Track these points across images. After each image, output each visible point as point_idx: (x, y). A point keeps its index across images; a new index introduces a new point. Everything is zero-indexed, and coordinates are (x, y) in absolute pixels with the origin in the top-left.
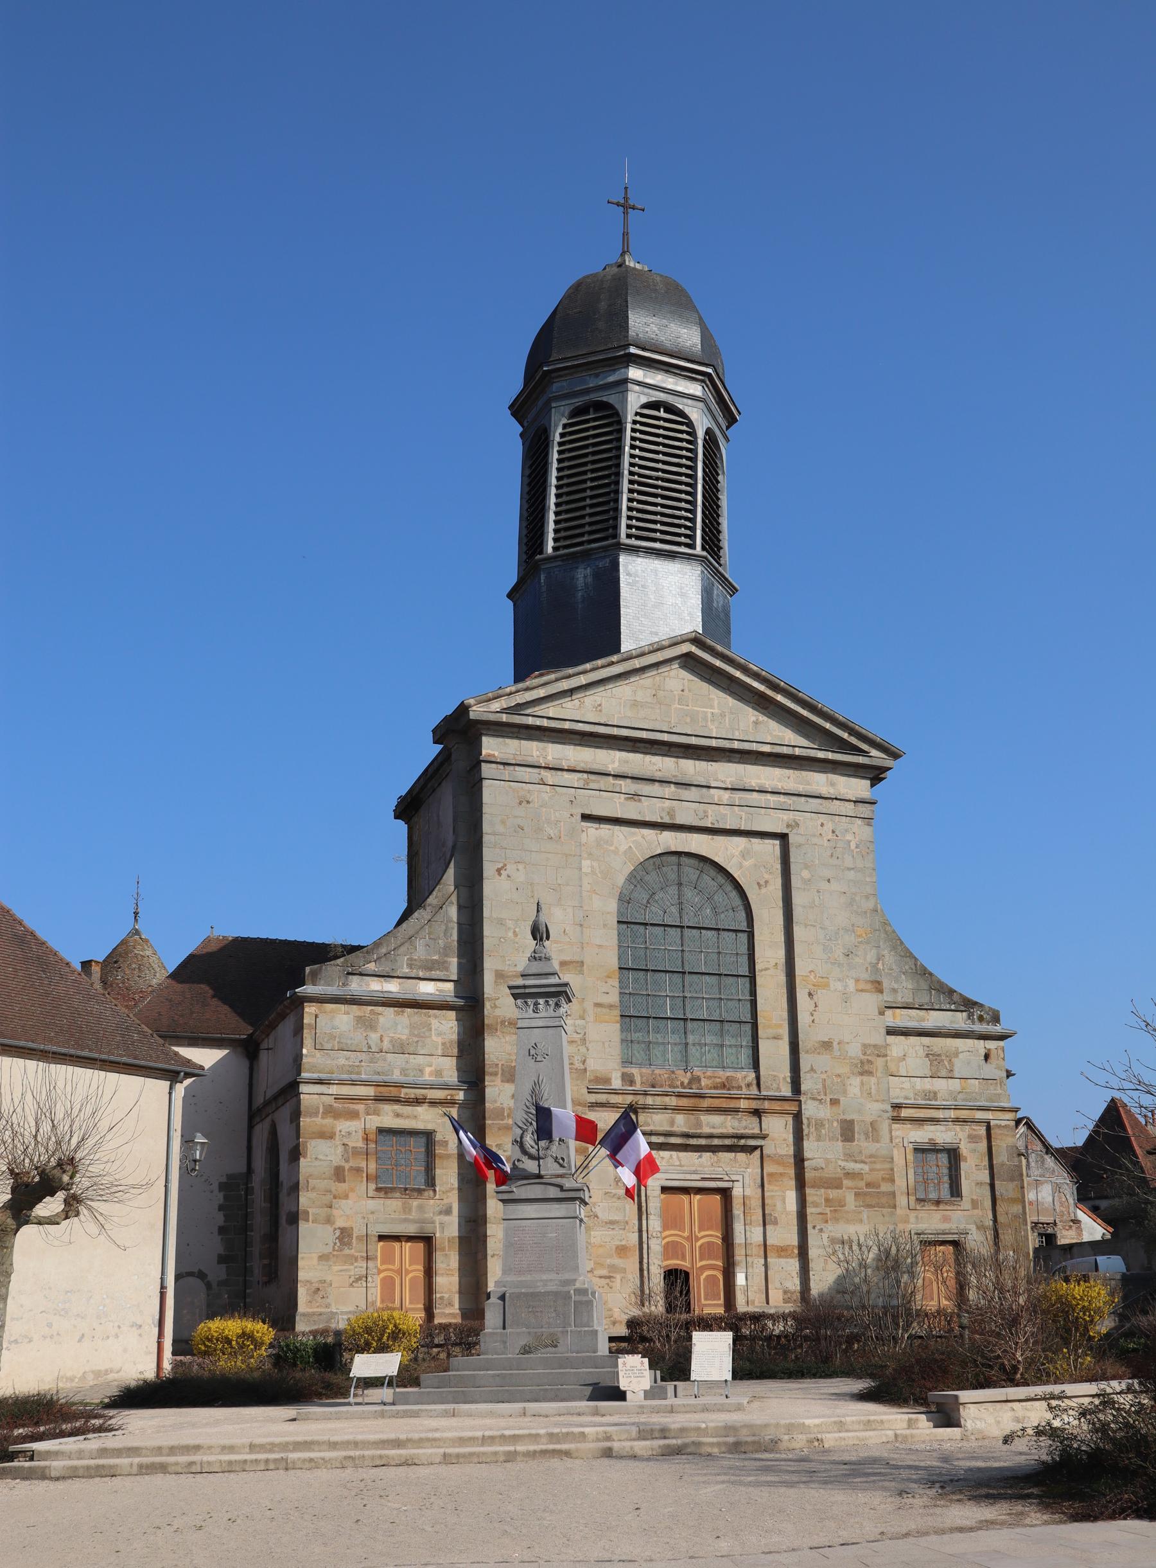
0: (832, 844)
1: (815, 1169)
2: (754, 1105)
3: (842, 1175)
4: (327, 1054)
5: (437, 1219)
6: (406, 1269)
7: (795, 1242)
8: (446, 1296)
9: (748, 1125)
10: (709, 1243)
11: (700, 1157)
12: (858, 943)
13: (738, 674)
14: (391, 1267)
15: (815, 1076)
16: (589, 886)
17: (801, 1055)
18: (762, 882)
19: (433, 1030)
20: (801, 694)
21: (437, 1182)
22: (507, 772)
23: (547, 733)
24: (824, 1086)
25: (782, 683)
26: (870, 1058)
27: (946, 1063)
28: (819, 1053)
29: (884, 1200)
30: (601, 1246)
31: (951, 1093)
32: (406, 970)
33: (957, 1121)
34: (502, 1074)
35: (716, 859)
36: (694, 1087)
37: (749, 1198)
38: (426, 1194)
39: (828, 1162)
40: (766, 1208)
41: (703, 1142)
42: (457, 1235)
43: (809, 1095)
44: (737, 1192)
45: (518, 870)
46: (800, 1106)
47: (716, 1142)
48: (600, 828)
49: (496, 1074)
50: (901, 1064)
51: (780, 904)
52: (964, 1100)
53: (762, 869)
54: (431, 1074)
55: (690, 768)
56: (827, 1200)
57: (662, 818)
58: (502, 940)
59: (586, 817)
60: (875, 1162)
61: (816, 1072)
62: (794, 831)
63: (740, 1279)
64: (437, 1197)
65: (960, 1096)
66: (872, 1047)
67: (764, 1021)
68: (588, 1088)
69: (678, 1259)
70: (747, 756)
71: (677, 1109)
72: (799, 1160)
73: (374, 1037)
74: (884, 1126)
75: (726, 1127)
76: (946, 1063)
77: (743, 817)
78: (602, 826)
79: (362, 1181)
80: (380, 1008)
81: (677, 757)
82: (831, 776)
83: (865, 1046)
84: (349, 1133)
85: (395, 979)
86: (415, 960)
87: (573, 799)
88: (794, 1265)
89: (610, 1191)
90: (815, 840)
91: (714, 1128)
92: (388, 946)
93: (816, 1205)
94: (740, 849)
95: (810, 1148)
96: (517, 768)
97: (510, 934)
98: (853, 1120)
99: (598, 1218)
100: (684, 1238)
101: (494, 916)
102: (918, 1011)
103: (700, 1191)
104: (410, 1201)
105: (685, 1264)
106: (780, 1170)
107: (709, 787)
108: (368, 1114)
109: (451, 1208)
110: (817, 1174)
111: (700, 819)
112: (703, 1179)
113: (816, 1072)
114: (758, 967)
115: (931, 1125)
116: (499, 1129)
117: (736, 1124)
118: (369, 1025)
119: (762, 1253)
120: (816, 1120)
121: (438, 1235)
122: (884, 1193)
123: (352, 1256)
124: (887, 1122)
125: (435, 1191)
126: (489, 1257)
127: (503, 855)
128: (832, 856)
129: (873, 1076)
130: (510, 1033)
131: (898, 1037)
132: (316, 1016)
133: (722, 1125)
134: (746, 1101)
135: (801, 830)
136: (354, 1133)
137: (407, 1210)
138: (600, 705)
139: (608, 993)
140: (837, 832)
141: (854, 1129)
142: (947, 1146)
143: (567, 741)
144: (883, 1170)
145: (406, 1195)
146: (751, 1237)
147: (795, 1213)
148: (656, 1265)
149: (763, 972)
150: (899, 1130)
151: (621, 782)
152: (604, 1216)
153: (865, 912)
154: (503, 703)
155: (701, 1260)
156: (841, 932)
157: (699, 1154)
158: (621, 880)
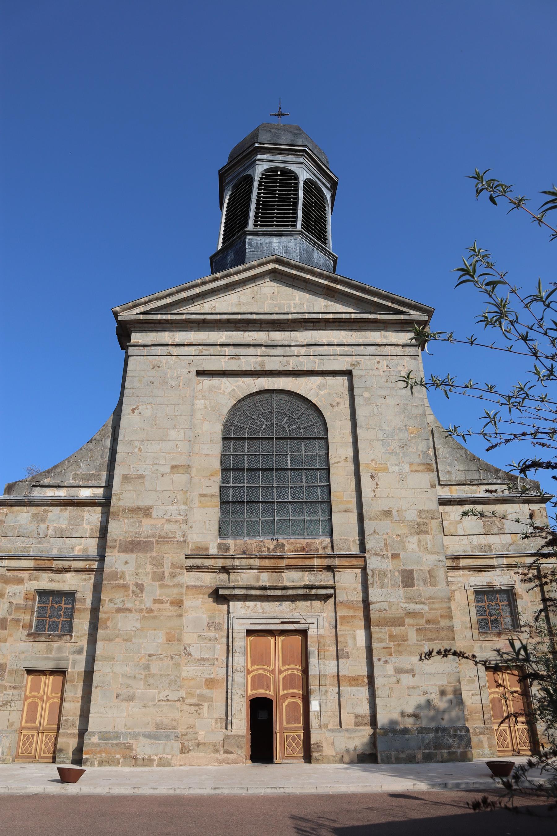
0: (386, 374)
1: (380, 611)
2: (326, 562)
3: (404, 615)
4: (9, 540)
5: (71, 657)
6: (47, 697)
7: (365, 673)
8: (71, 718)
9: (325, 578)
10: (290, 675)
11: (281, 605)
12: (411, 437)
13: (308, 276)
14: (36, 694)
15: (378, 537)
16: (202, 416)
17: (365, 522)
18: (334, 404)
19: (85, 520)
20: (353, 281)
21: (74, 629)
22: (145, 351)
23: (174, 325)
24: (386, 545)
25: (339, 277)
26: (425, 521)
27: (498, 523)
28: (381, 520)
29: (443, 634)
30: (192, 679)
31: (503, 545)
32: (71, 482)
33: (509, 566)
34: (119, 546)
35: (299, 392)
36: (278, 551)
37: (324, 637)
38: (64, 638)
39: (391, 604)
40: (339, 644)
41: (279, 592)
42: (83, 669)
43: (373, 552)
44: (312, 632)
45: (147, 409)
46: (365, 561)
47: (290, 592)
48: (212, 380)
49: (114, 547)
50: (458, 526)
51: (349, 417)
52: (514, 550)
53: (335, 396)
54: (79, 551)
55: (277, 337)
56: (391, 636)
57: (255, 368)
58: (130, 454)
59: (200, 373)
60: (433, 603)
61: (378, 534)
62: (357, 368)
63: (314, 706)
64: (73, 640)
65: (511, 548)
66: (426, 513)
67: (336, 499)
68: (186, 555)
69: (263, 689)
70: (318, 324)
71: (261, 569)
72: (366, 603)
73: (43, 526)
74: (441, 573)
75: (304, 581)
76: (498, 523)
77: (317, 363)
78: (213, 378)
79: (18, 629)
80: (51, 508)
81: (268, 331)
82: (383, 333)
83: (420, 512)
84: (15, 594)
85: (64, 488)
86: (79, 475)
87: (191, 362)
88: (364, 692)
89: (203, 634)
90: (373, 372)
91: (293, 582)
92: (62, 467)
93: (380, 640)
94: (317, 384)
95: (374, 594)
96: (153, 348)
97: (136, 450)
98: (412, 570)
99: (191, 656)
100: (269, 671)
101: (126, 439)
102: (470, 487)
103: (282, 632)
104: (52, 644)
105: (269, 693)
106: (351, 613)
107: (290, 346)
108: (30, 580)
109: (82, 648)
110: (382, 615)
111: (284, 366)
112: (283, 623)
113: (378, 534)
114: (331, 462)
115: (488, 571)
116: (113, 587)
117: (312, 578)
118: (42, 519)
119: (336, 682)
120: (379, 571)
121: (69, 670)
122: (443, 628)
123: (4, 686)
124: (443, 570)
125: (71, 636)
126: (93, 689)
127: (137, 400)
128: (387, 381)
129: (429, 534)
130: (128, 517)
131: (455, 506)
132: (6, 515)
133: (301, 579)
134: (319, 560)
135: (362, 367)
136: (18, 594)
137: (49, 650)
138: (214, 307)
139: (211, 487)
140: (390, 366)
141: (414, 576)
142: (504, 587)
143: (189, 329)
144: (441, 609)
145: (49, 639)
146: (324, 670)
147: (365, 648)
148: (239, 695)
149: (336, 465)
150: (457, 577)
151: (226, 349)
152: (196, 653)
153: (416, 417)
154: (142, 309)
155: (283, 690)
156: (396, 431)
157: (280, 603)
158: (225, 410)
